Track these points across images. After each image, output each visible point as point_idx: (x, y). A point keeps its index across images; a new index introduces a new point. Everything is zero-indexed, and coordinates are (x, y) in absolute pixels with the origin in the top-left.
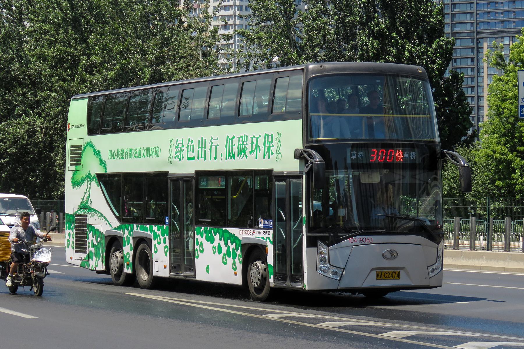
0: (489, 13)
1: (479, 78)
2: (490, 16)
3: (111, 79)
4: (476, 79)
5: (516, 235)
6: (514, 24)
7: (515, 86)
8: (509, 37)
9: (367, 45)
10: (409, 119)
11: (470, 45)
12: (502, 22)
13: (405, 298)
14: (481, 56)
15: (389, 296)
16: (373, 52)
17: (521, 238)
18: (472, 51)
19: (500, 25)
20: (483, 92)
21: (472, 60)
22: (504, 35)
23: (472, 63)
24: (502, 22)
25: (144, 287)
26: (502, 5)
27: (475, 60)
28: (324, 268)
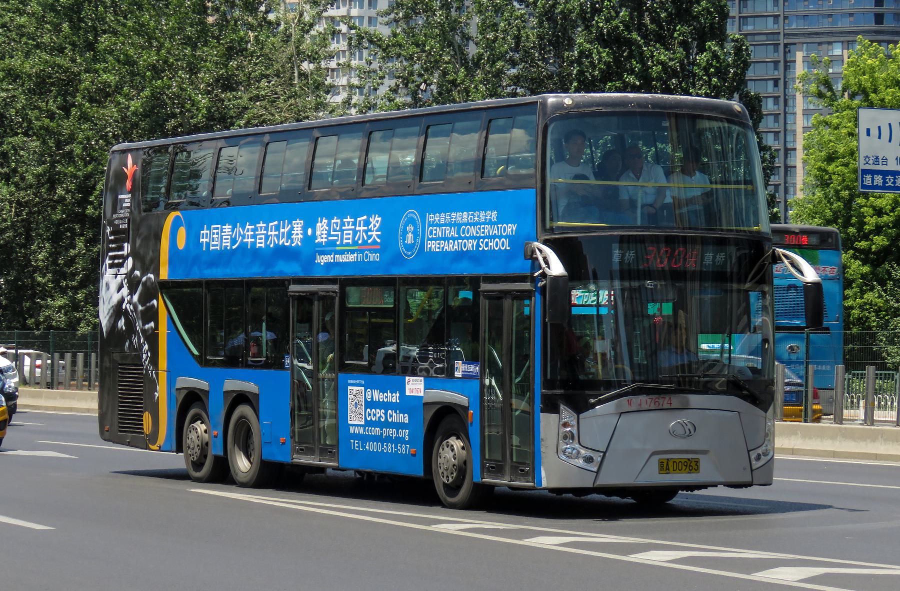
1: (788, 116)
2: (808, 5)
3: (135, 113)
4: (782, 117)
5: (852, 396)
6: (852, 19)
7: (851, 134)
8: (842, 42)
10: (720, 192)
11: (771, 56)
12: (830, 16)
13: (703, 504)
14: (791, 76)
15: (676, 501)
16: (600, 69)
17: (862, 403)
18: (776, 68)
19: (826, 20)
20: (795, 141)
21: (776, 84)
22: (832, 39)
23: (776, 88)
24: (830, 16)
25: (243, 485)
27: (781, 83)
28: (570, 450)
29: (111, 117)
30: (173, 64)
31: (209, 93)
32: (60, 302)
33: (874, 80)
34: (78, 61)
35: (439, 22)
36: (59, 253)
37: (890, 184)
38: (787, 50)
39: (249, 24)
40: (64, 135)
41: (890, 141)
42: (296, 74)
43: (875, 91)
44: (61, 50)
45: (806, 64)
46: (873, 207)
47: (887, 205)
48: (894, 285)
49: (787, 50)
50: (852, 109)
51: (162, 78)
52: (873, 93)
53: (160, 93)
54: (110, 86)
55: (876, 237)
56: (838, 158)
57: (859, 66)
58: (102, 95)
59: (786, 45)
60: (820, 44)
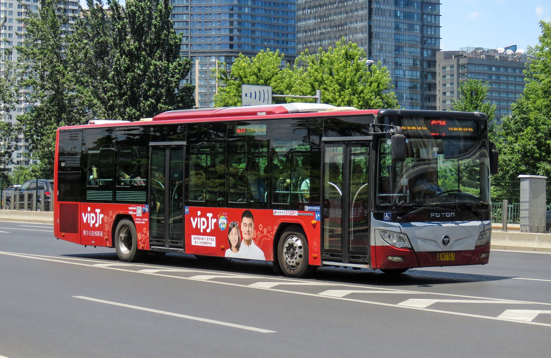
0: (200, 37)
6: (219, 46)
8: (216, 56)
9: (119, 60)
12: (210, 45)
16: (124, 67)
24: (210, 45)
41: (255, 99)
43: (246, 77)
59: (191, 57)
60: (206, 57)
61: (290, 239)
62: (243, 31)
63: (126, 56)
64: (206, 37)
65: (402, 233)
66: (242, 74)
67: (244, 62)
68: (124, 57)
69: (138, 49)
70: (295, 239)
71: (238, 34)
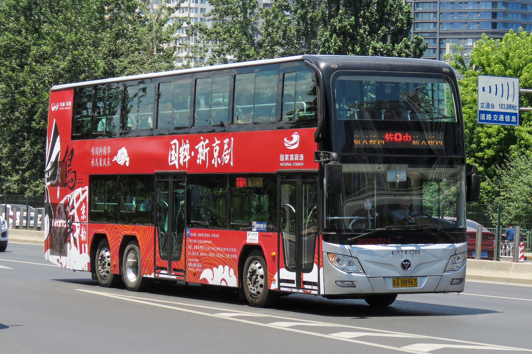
0: (452, 13)
2: (454, 17)
6: (478, 25)
7: (474, 90)
8: (473, 38)
12: (466, 23)
18: (434, 52)
19: (464, 26)
24: (466, 23)
26: (466, 5)
29: (48, 71)
30: (84, 41)
31: (105, 59)
32: (16, 177)
33: (488, 59)
34: (29, 39)
35: (240, 21)
36: (15, 150)
37: (495, 119)
38: (441, 42)
39: (129, 20)
40: (20, 81)
42: (155, 49)
43: (489, 66)
44: (20, 32)
45: (452, 50)
46: (487, 133)
47: (494, 132)
48: (497, 178)
49: (441, 42)
50: (475, 76)
51: (77, 50)
52: (487, 66)
53: (77, 58)
54: (47, 54)
55: (488, 150)
56: (467, 104)
57: (480, 51)
58: (42, 59)
59: (440, 39)
60: (460, 39)
61: (253, 264)
62: (510, 5)
63: (338, 36)
64: (460, 13)
65: (352, 256)
66: (485, 62)
67: (488, 45)
68: (334, 36)
69: (356, 26)
70: (259, 265)
71: (504, 8)
